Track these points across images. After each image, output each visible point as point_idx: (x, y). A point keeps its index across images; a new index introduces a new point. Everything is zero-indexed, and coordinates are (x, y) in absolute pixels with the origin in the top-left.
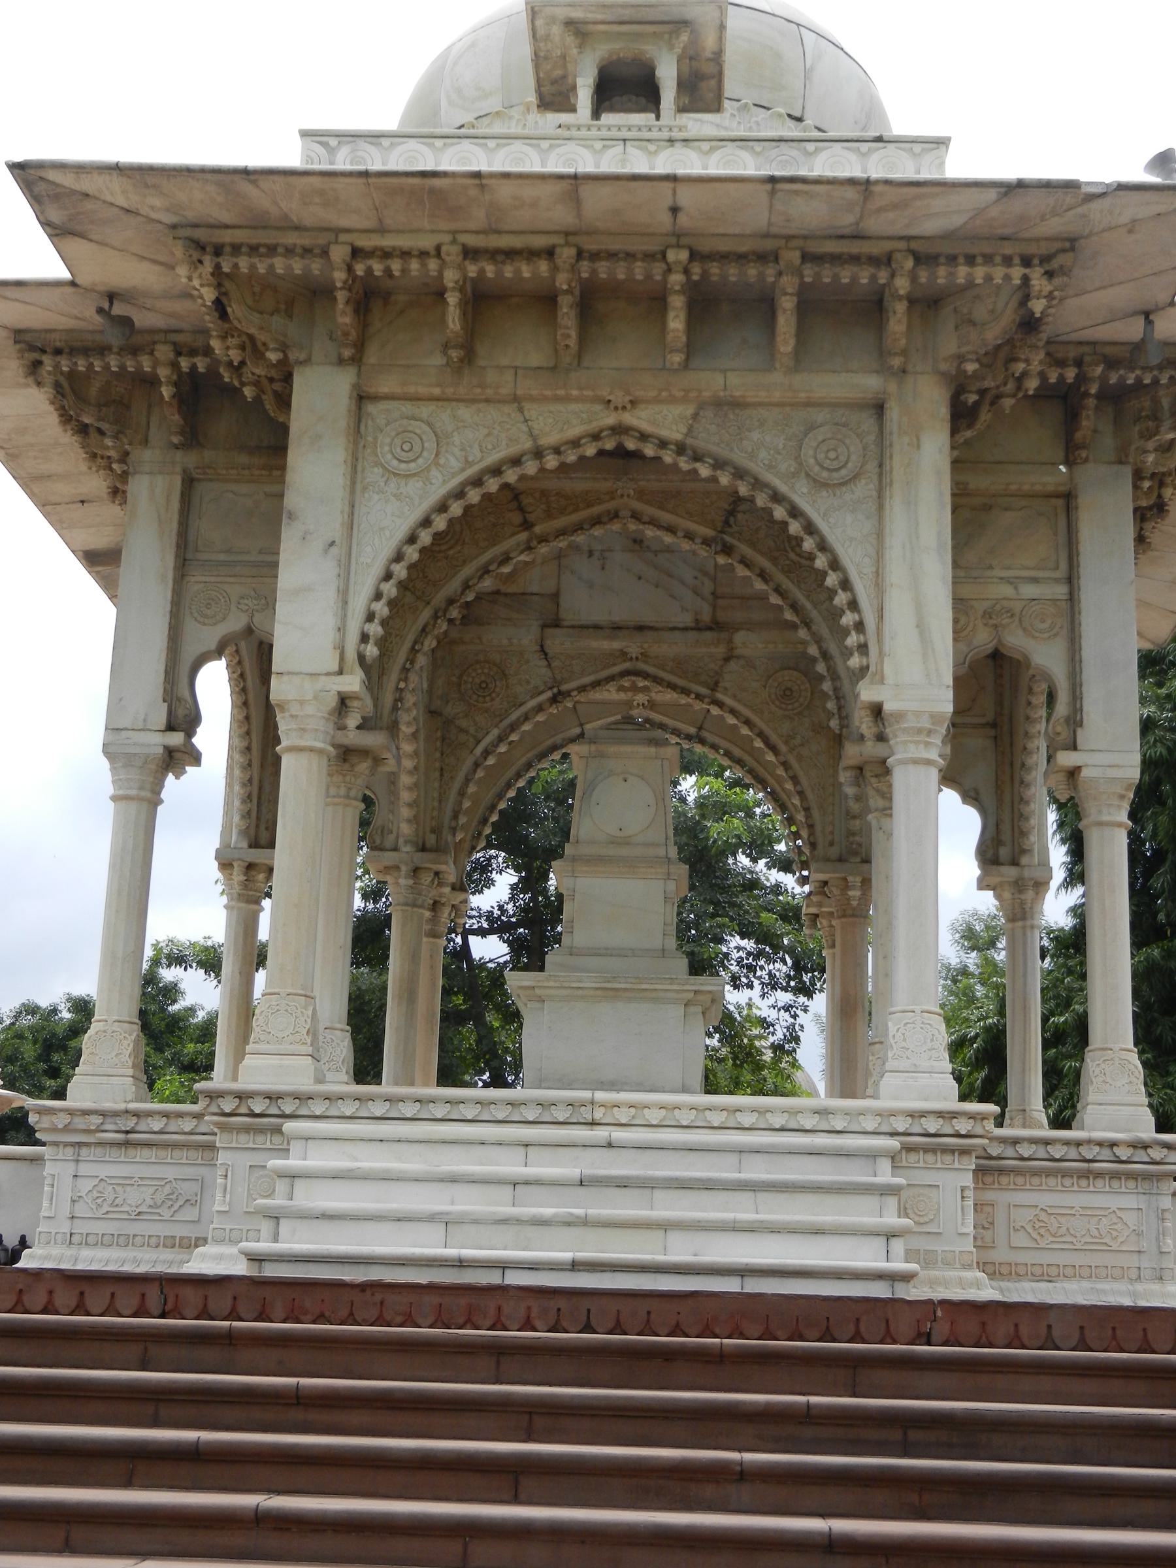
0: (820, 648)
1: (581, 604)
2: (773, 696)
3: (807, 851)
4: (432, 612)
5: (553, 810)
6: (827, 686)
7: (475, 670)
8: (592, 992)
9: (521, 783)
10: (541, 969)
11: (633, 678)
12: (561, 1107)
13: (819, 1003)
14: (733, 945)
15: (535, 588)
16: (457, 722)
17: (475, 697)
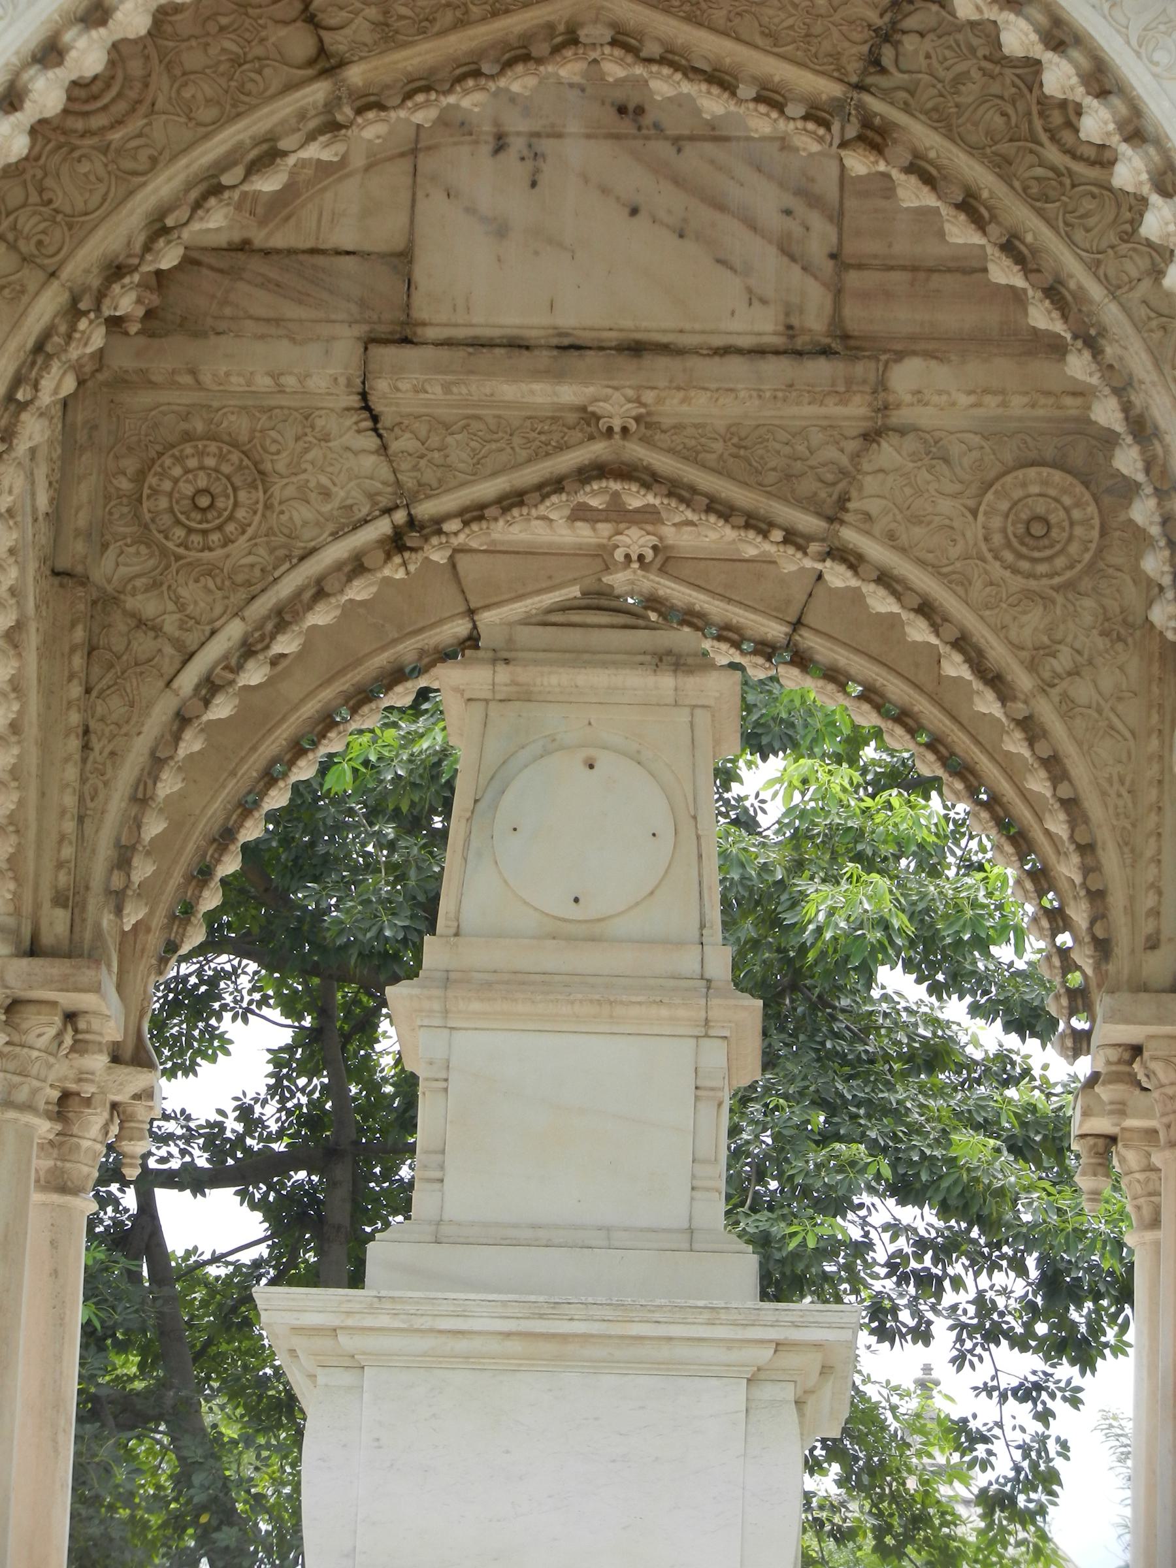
0: (1126, 408)
1: (474, 277)
2: (997, 539)
4: (64, 297)
5: (392, 846)
8: (494, 1346)
9: (305, 771)
10: (356, 1280)
11: (615, 486)
14: (879, 1218)
15: (345, 237)
16: (131, 603)
17: (179, 533)
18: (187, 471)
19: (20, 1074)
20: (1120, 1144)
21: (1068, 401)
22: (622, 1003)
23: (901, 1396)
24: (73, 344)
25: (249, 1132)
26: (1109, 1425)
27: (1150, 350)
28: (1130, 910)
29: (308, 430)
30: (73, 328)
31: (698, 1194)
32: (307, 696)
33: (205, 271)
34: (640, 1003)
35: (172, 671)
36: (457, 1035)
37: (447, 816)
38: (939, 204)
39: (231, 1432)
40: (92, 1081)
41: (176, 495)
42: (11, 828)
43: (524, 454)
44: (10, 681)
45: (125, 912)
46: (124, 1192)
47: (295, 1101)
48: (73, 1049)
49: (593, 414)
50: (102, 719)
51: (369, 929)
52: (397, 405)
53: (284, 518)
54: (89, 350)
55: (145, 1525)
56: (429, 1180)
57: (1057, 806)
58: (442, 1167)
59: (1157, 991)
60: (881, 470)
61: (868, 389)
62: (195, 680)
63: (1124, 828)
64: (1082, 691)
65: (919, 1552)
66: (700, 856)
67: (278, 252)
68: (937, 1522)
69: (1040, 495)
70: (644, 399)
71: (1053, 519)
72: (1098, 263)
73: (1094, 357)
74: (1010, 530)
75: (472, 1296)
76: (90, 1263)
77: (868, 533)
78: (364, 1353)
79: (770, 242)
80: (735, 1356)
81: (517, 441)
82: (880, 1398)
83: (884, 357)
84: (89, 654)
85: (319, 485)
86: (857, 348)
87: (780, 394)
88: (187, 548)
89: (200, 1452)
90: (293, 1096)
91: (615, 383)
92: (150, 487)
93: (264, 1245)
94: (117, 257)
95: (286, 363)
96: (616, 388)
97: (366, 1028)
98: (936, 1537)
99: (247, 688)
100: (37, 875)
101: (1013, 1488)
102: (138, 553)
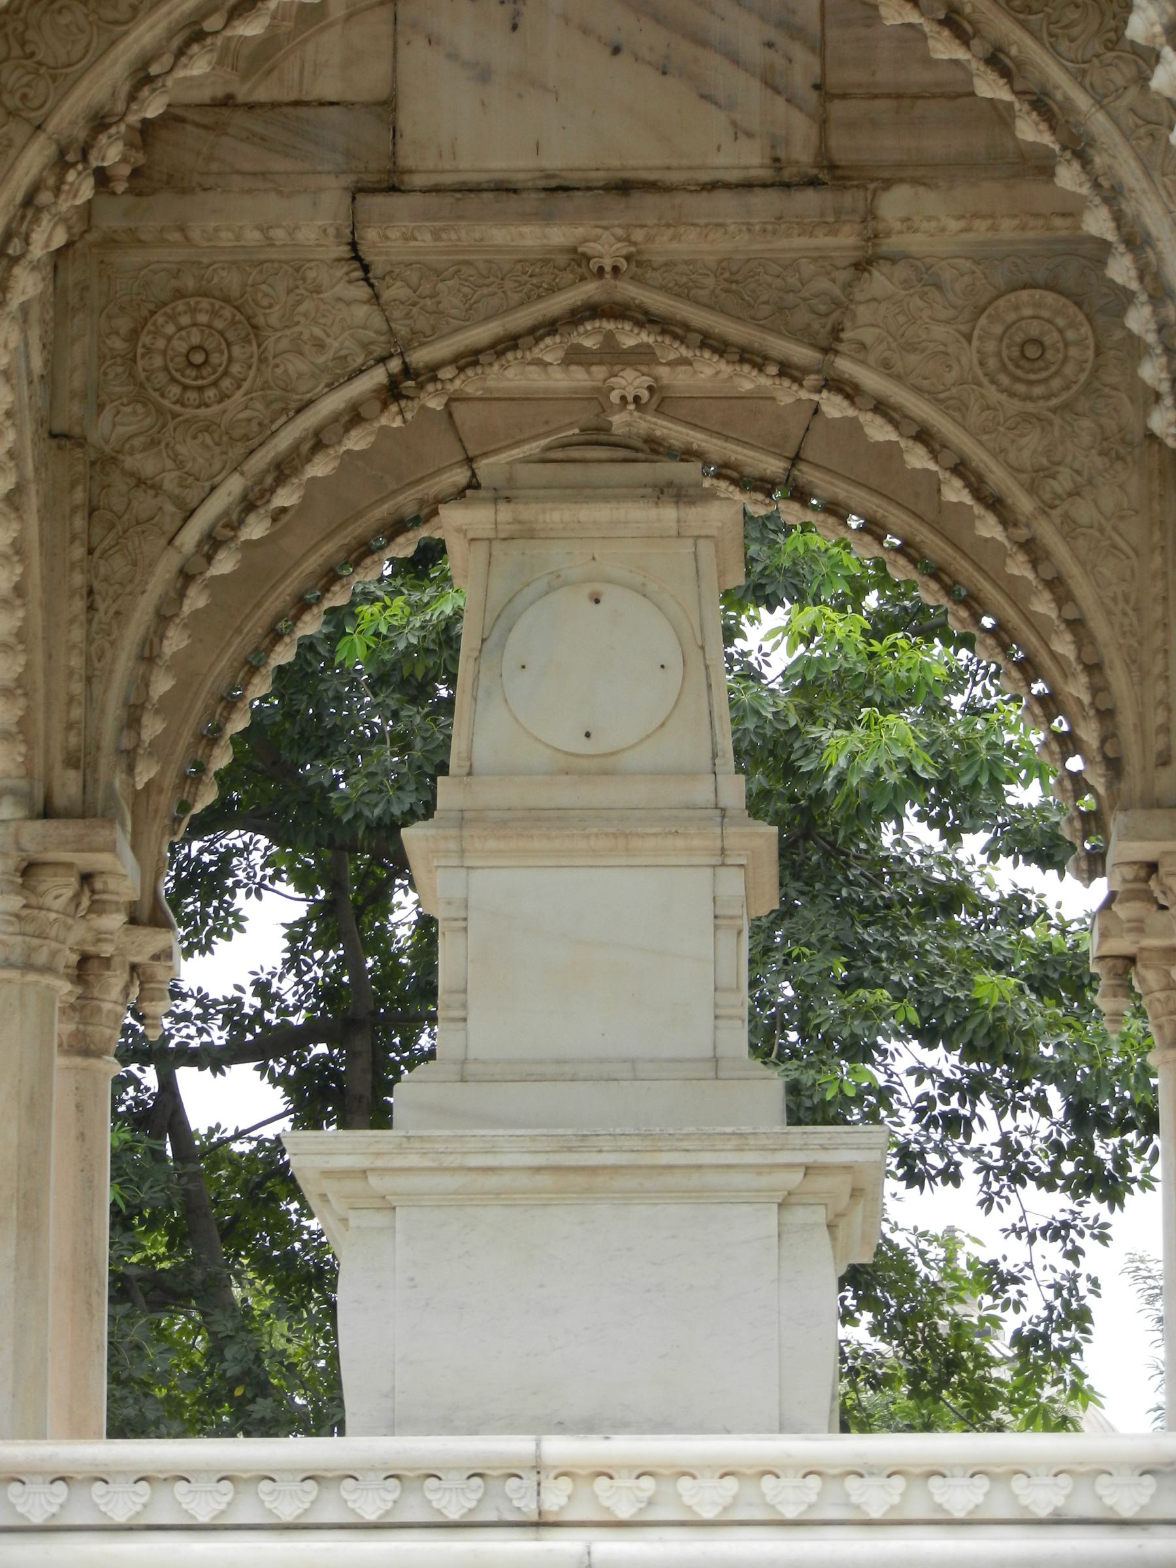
0: (1118, 218)
1: (460, 123)
2: (992, 363)
3: (1098, 782)
4: (52, 150)
5: (395, 715)
6: (1139, 319)
7: (172, 318)
8: (524, 1181)
9: (311, 626)
10: (381, 1118)
11: (609, 325)
12: (453, 1480)
13: (1140, 1220)
14: (900, 1065)
15: (329, 88)
16: (129, 462)
17: (175, 390)
18: (181, 329)
19: (38, 937)
20: (1139, 965)
21: (1058, 222)
22: (638, 835)
23: (930, 1242)
24: (63, 197)
25: (267, 1006)
26: (1136, 1267)
27: (1139, 158)
28: (1140, 727)
29: (300, 283)
30: (61, 180)
31: (721, 1023)
32: (309, 550)
33: (189, 127)
34: (655, 835)
35: (173, 529)
36: (476, 875)
37: (452, 682)
38: (922, 20)
39: (260, 1306)
40: (112, 941)
41: (170, 353)
42: (20, 691)
43: (516, 298)
44: (13, 544)
45: (137, 770)
46: (143, 1071)
47: (312, 975)
48: (90, 910)
49: (584, 255)
50: (106, 579)
51: (376, 805)
52: (387, 253)
53: (279, 371)
54: (79, 201)
55: (180, 1404)
56: (453, 1020)
57: (1063, 627)
58: (464, 1006)
59: (1170, 807)
60: (874, 299)
61: (858, 219)
62: (197, 537)
63: (1131, 646)
64: (1083, 511)
65: (954, 1396)
66: (709, 686)
67: (262, 105)
68: (971, 1365)
69: (1034, 317)
70: (633, 238)
71: (1047, 341)
72: (1084, 73)
73: (1083, 166)
74: (1005, 353)
75: (501, 1132)
76: (116, 1144)
77: (863, 362)
78: (395, 1194)
79: (753, 75)
80: (765, 1181)
81: (509, 284)
82: (908, 1245)
83: (872, 186)
84: (90, 515)
85: (313, 337)
86: (844, 178)
87: (769, 227)
88: (183, 405)
89: (230, 1325)
90: (310, 970)
91: (605, 223)
92: (144, 346)
93: (287, 1118)
94: (102, 108)
95: (273, 219)
96: (606, 228)
97: (380, 902)
98: (971, 1379)
99: (249, 544)
100: (47, 738)
101: (1047, 1327)
102: (135, 412)
